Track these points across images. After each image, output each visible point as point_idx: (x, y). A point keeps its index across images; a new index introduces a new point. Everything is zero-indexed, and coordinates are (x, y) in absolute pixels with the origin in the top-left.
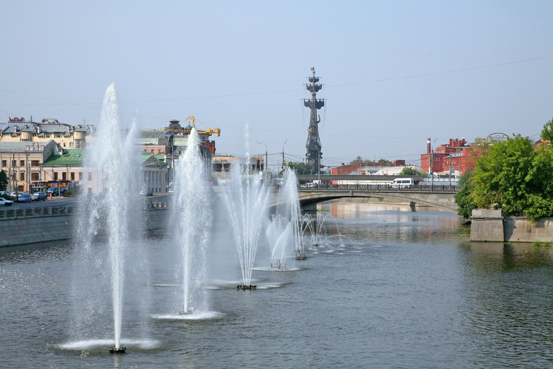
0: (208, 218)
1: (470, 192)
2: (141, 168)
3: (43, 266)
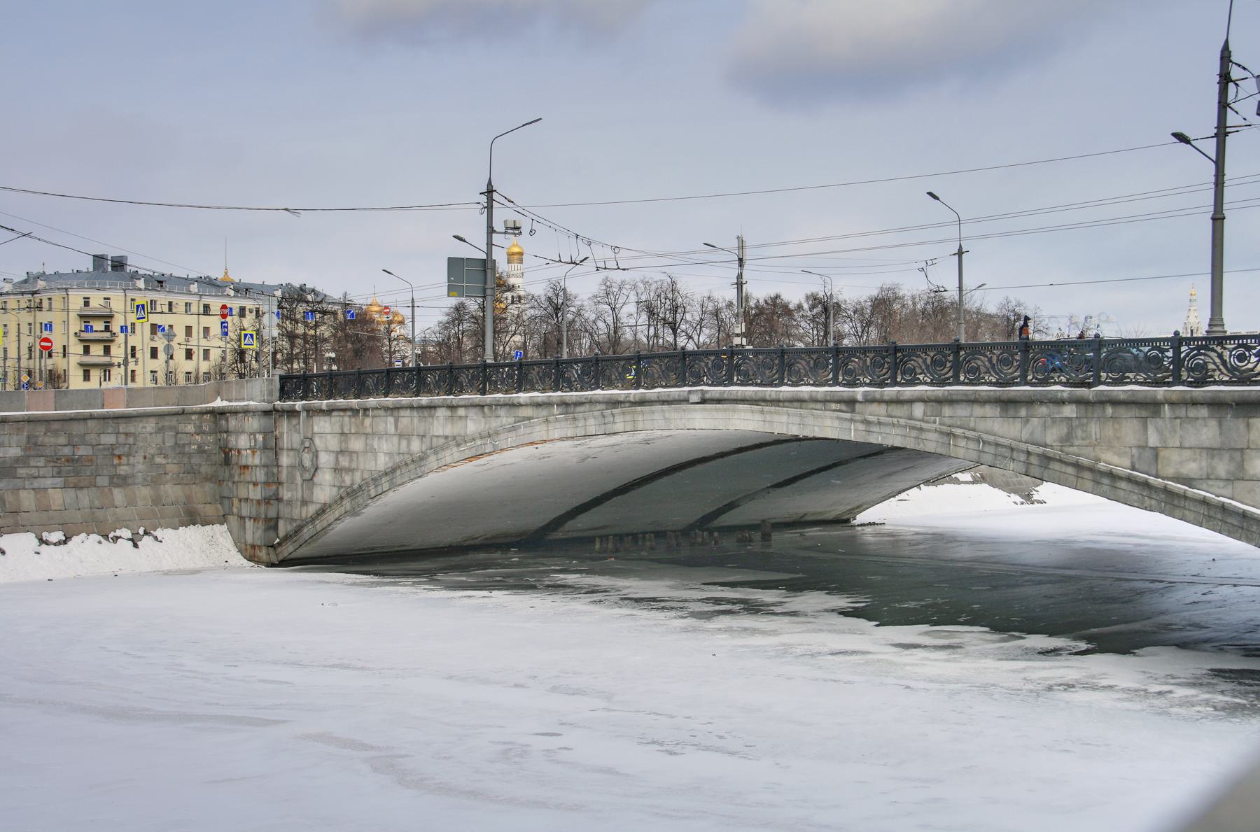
0: (118, 538)
1: (1113, 447)
2: (1024, 312)
3: (774, 371)
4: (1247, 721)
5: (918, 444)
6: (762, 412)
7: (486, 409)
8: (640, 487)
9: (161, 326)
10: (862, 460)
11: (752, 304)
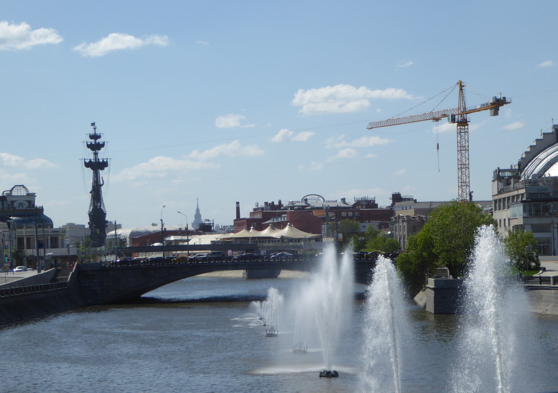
10: (484, 111)
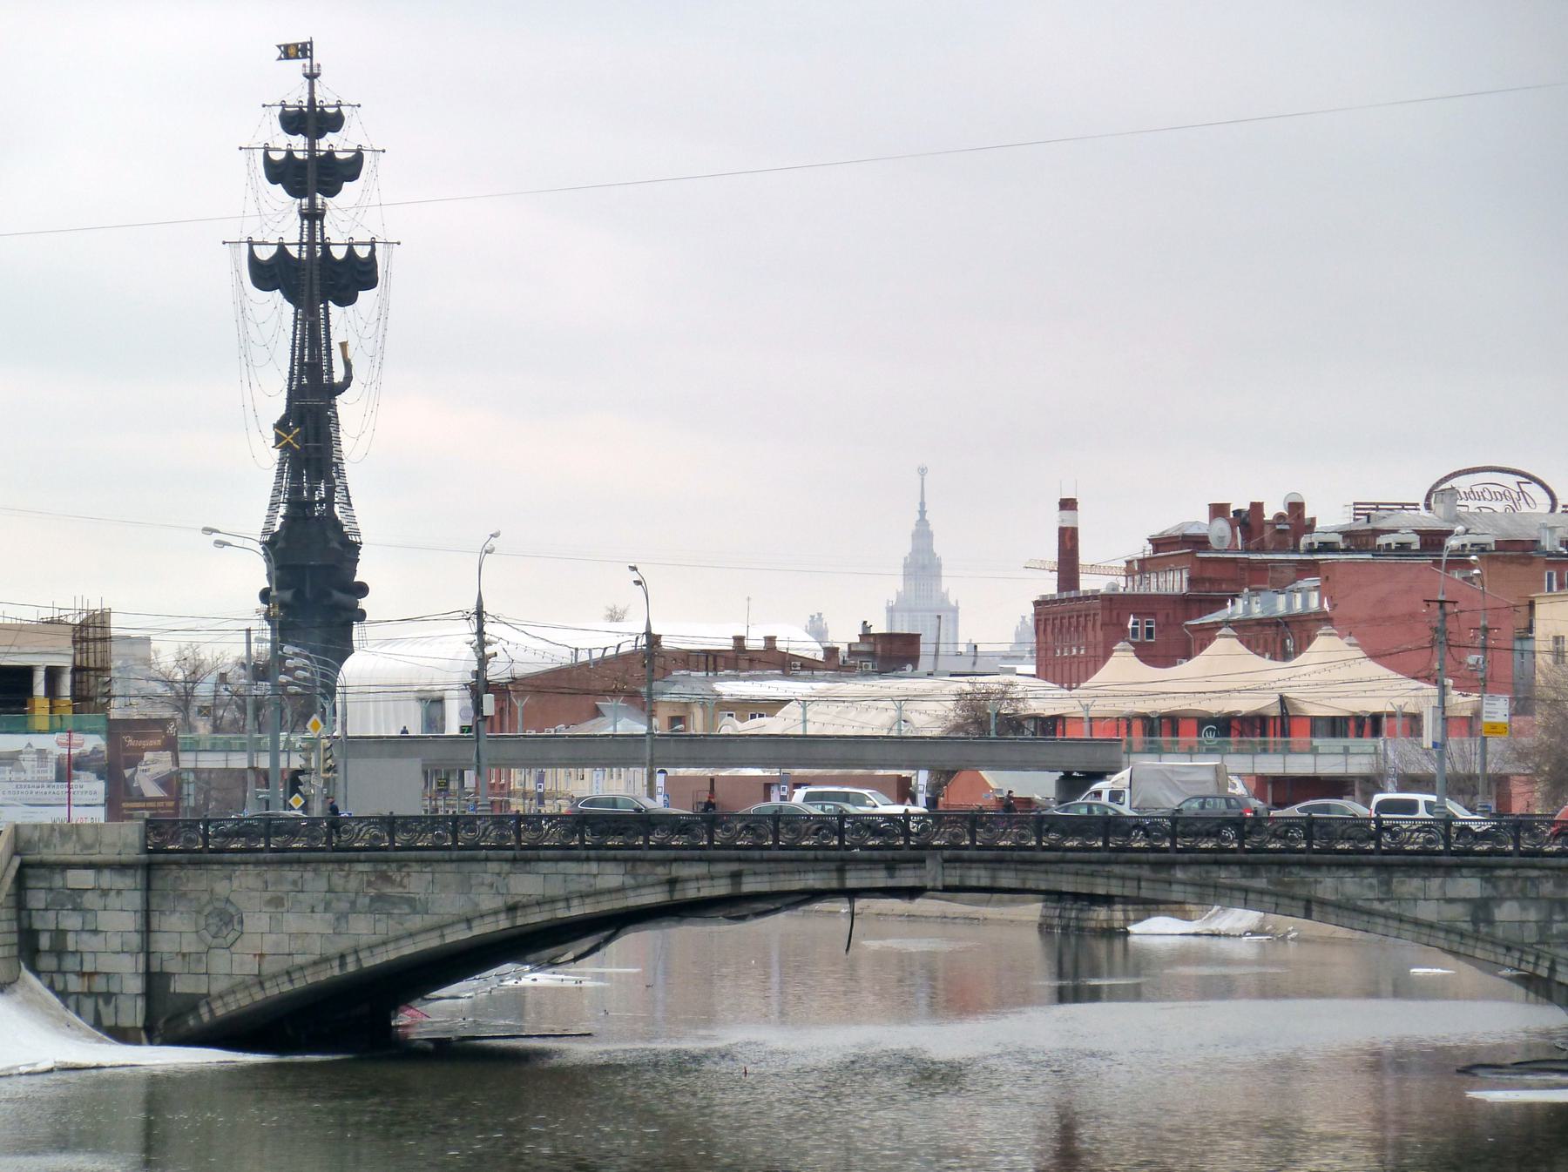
4: (946, 718)
5: (442, 936)
6: (1016, 870)
7: (1252, 896)
8: (394, 756)
9: (351, 505)
11: (128, 773)
